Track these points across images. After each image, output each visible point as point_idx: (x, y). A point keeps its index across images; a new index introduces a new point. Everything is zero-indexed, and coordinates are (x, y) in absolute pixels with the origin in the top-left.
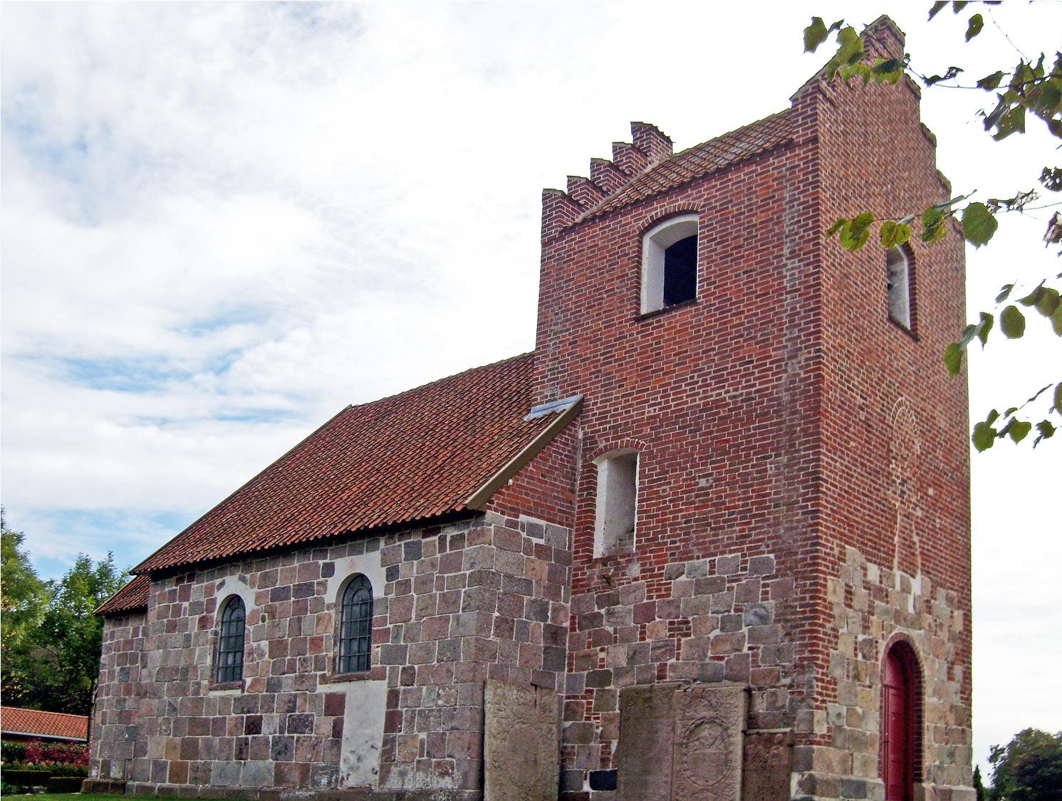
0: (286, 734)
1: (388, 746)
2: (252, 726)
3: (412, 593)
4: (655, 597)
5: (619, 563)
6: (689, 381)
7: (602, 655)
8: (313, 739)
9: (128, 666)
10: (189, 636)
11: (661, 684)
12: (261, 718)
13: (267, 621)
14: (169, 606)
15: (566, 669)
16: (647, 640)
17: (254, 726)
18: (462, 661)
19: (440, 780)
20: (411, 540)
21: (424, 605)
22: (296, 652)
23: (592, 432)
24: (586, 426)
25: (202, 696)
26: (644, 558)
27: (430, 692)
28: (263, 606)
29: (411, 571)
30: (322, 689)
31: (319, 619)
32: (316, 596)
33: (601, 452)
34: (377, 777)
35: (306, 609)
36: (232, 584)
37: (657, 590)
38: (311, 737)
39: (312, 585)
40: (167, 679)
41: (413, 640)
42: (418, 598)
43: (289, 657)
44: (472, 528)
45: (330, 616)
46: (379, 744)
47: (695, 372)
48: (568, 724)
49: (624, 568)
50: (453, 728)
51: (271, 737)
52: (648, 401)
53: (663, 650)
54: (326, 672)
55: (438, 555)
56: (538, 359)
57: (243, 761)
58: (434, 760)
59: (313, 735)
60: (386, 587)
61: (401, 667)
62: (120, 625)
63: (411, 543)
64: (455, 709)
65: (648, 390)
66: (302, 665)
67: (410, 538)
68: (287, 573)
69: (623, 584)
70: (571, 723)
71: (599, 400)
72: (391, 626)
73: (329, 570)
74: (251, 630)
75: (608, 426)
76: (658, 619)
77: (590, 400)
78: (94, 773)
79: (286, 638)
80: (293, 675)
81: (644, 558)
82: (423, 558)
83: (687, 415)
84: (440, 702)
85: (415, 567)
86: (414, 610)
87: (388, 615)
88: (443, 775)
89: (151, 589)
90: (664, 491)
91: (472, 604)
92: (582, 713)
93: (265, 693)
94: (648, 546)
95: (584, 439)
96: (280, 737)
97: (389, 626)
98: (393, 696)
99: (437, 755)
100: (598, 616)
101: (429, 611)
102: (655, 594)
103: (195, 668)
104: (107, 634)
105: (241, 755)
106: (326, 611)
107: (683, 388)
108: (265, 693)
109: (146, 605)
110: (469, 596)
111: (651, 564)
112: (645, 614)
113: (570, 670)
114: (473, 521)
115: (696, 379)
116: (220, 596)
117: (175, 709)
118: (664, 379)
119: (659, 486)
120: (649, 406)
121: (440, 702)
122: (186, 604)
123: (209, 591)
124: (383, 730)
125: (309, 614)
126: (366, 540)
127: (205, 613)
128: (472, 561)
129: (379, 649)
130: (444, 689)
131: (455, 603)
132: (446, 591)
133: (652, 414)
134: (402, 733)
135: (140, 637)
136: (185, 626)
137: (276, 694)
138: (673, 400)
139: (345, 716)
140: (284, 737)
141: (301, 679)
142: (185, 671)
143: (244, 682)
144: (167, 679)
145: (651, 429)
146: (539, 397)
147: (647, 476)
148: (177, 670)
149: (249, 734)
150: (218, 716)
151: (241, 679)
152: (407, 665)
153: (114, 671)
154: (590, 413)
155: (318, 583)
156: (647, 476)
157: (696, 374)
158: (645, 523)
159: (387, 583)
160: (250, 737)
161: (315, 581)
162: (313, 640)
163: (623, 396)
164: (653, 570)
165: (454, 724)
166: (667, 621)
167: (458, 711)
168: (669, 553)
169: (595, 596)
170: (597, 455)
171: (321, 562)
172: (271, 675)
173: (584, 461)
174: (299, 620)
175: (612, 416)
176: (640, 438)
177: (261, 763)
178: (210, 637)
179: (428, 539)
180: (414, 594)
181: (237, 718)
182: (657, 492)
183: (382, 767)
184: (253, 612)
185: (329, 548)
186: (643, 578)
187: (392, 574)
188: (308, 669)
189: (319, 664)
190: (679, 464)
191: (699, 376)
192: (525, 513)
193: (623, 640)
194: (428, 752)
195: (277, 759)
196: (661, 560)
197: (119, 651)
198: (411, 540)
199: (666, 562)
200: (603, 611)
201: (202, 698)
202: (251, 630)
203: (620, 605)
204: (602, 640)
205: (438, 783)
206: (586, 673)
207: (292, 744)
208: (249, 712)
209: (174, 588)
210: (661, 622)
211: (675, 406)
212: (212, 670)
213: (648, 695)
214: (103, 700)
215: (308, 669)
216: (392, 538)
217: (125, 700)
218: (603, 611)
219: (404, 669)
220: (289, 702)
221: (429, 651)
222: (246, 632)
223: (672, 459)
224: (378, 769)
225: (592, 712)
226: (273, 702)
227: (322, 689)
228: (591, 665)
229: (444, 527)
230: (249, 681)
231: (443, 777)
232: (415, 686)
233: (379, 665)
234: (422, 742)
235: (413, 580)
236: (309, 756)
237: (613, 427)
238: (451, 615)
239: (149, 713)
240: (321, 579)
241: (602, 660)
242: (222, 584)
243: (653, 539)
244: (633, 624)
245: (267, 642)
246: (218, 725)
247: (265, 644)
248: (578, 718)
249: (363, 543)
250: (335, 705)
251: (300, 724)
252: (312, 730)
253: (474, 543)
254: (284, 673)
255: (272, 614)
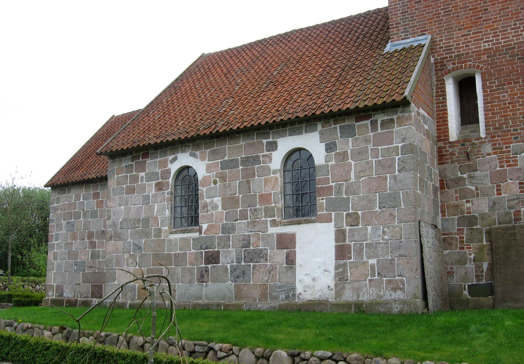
0: (243, 263)
1: (341, 270)
2: (211, 258)
3: (350, 160)
4: (505, 166)
5: (474, 144)
6: (513, 27)
7: (469, 205)
8: (268, 267)
9: (73, 220)
10: (148, 196)
11: (518, 224)
12: (218, 252)
13: (219, 183)
14: (127, 176)
15: (440, 215)
16: (503, 195)
17: (213, 258)
18: (403, 207)
19: (393, 293)
20: (346, 123)
21: (362, 169)
22: (247, 205)
23: (441, 59)
24: (436, 55)
25: (163, 238)
26: (494, 141)
27: (375, 230)
28: (214, 173)
29: (349, 145)
30: (273, 230)
31: (266, 181)
32: (262, 164)
33: (449, 72)
34: (333, 292)
35: (254, 174)
36: (184, 159)
37: (507, 162)
38: (266, 265)
39: (258, 157)
40: (130, 227)
41: (354, 193)
42: (355, 164)
43: (240, 209)
44: (400, 115)
45: (277, 179)
46: (332, 269)
47: (517, 21)
48: (446, 252)
49: (479, 147)
50: (400, 256)
51: (229, 266)
52: (482, 39)
53: (516, 201)
54: (276, 218)
55: (371, 134)
56: (391, 12)
57: (204, 284)
58: (385, 279)
59: (268, 263)
60: (326, 157)
61: (345, 213)
62: (64, 193)
63: (346, 125)
64: (401, 242)
65: (481, 32)
66: (253, 214)
67: (344, 122)
68: (236, 150)
69: (479, 157)
70: (448, 251)
71: (443, 39)
72: (333, 184)
73: (273, 146)
74: (204, 190)
75: (453, 55)
76: (510, 181)
77: (437, 38)
78: (50, 294)
79: (237, 195)
80: (245, 221)
81: (494, 141)
82: (357, 136)
83: (514, 48)
84: (386, 237)
85: (350, 143)
86: (352, 173)
87: (330, 176)
88: (394, 289)
89: (109, 165)
90: (504, 96)
91: (407, 166)
92: (457, 244)
93: (221, 235)
94: (496, 133)
95: (435, 63)
96: (237, 266)
97: (331, 184)
98: (340, 235)
99: (387, 275)
100: (460, 180)
101: (367, 173)
102: (505, 165)
103: (156, 219)
104: (53, 200)
105: (202, 279)
106: (272, 175)
107: (509, 31)
108: (221, 235)
109: (106, 175)
110: (403, 162)
111: (499, 144)
112: (499, 178)
113: (443, 215)
114: (400, 109)
115: (518, 25)
116: (174, 168)
117: (140, 248)
118: (493, 26)
119: (500, 93)
120: (484, 42)
121: (386, 237)
122: (143, 174)
123: (164, 164)
124: (334, 258)
125: (256, 177)
126: (304, 125)
127: (160, 180)
128: (403, 137)
129: (324, 201)
130: (388, 228)
131: (391, 166)
132: (380, 158)
133: (487, 47)
134: (352, 260)
135: (81, 200)
136: (143, 189)
137: (231, 235)
138: (502, 39)
139: (297, 249)
140: (241, 265)
141: (253, 223)
142: (146, 221)
143: (201, 228)
144: (130, 227)
145: (487, 57)
146: (395, 37)
147: (489, 87)
148: (139, 221)
149: (209, 264)
150: (179, 252)
151: (198, 225)
152: (351, 211)
153: (61, 224)
154: (438, 47)
155: (263, 156)
156: (489, 87)
157: (518, 23)
158: (491, 118)
159: (327, 154)
160: (209, 266)
161: (261, 154)
162: (261, 196)
163: (462, 36)
164: (502, 148)
165: (402, 252)
166: (517, 182)
167: (404, 243)
168: (513, 137)
169: (458, 166)
170: (446, 73)
171: (264, 141)
172: (225, 222)
173: (437, 77)
174: (248, 182)
175: (456, 48)
176: (479, 62)
177: (222, 285)
178: (167, 196)
179: (361, 123)
180: (352, 161)
181: (197, 253)
182: (499, 97)
183: (336, 285)
184: (204, 178)
185: (271, 131)
186: (494, 153)
187: (330, 148)
188: (259, 216)
189: (269, 212)
190: (513, 79)
191: (520, 24)
192: (423, 109)
193: (484, 195)
194: (379, 274)
195: (236, 282)
196: (508, 143)
197: (65, 210)
198: (346, 123)
199: (512, 143)
200: (465, 176)
201: (164, 240)
202: (204, 190)
203: (479, 172)
204: (465, 195)
205: (391, 295)
206: (456, 217)
207: (249, 270)
208: (207, 248)
209: (131, 163)
210: (513, 183)
211: (504, 42)
212: (171, 219)
213: (512, 232)
214: (54, 244)
215: (259, 216)
216: (328, 123)
217: (71, 244)
218: (465, 176)
219: (348, 215)
220: (244, 240)
221: (371, 201)
222: (200, 192)
223: (507, 76)
224: (332, 286)
225: (465, 244)
226: (229, 240)
227: (273, 230)
228: (460, 212)
229: (374, 115)
230: (205, 226)
231: (395, 291)
232: (360, 226)
233: (325, 212)
234: (372, 266)
235: (349, 151)
236: (266, 278)
237: (458, 56)
238: (388, 175)
239: (117, 251)
240: (266, 153)
241: (469, 208)
242: (175, 159)
243: (499, 128)
244: (490, 184)
245: (220, 198)
246: (180, 259)
247: (217, 200)
248: (453, 247)
249: (302, 127)
250: (287, 243)
251: (256, 256)
252: (266, 259)
253: (402, 125)
254: (237, 220)
255: (223, 178)
